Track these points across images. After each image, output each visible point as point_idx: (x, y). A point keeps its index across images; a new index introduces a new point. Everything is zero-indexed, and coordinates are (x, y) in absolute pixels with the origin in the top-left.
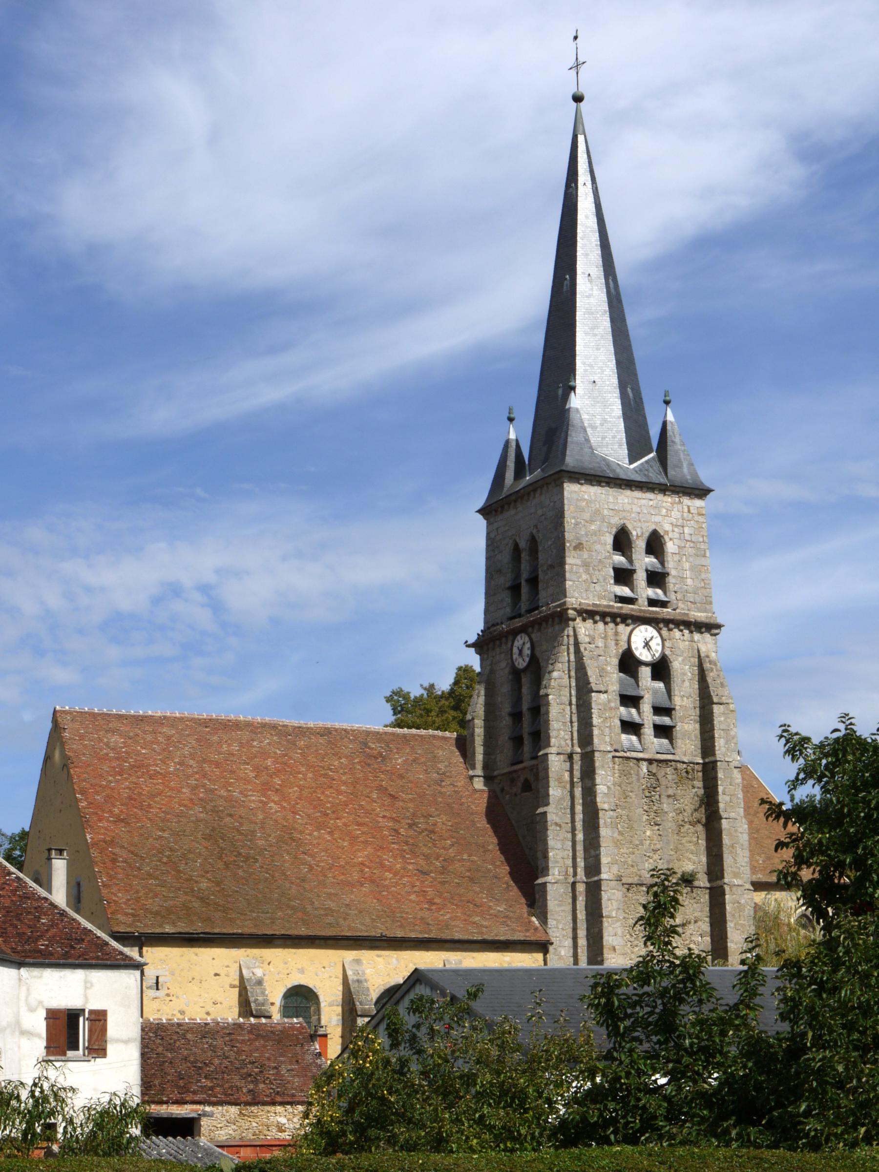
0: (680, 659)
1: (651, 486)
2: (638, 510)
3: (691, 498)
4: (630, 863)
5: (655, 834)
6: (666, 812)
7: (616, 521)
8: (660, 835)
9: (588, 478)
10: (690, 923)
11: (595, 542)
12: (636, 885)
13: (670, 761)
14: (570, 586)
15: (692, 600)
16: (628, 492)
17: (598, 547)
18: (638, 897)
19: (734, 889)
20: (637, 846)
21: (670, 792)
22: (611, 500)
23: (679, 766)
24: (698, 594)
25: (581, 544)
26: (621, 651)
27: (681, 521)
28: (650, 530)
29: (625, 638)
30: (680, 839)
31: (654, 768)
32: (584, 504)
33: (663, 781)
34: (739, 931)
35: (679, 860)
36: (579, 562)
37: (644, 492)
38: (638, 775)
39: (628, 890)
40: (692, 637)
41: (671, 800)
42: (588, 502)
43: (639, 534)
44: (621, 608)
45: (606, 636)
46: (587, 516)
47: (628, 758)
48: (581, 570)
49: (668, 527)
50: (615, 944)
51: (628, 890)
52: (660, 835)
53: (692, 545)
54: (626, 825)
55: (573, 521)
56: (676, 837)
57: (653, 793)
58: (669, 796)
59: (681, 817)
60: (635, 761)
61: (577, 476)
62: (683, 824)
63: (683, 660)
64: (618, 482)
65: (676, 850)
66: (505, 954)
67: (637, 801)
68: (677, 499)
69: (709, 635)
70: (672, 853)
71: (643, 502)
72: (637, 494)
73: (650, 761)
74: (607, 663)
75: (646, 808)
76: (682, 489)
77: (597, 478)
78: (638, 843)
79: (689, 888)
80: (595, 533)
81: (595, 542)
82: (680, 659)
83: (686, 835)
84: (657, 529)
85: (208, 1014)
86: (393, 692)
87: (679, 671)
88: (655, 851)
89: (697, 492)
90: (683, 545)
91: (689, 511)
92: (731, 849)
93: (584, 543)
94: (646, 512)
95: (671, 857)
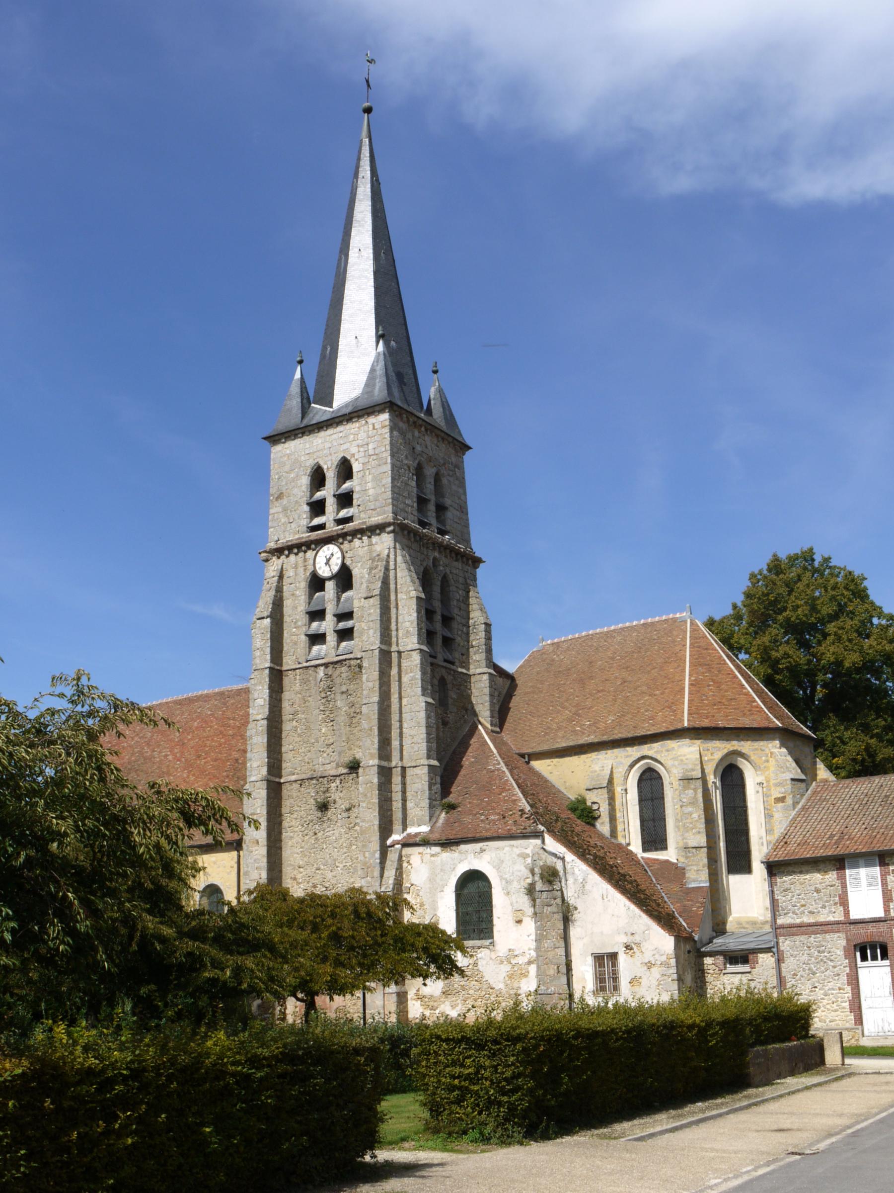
0: (359, 565)
1: (337, 420)
2: (330, 445)
3: (376, 416)
4: (307, 760)
5: (329, 730)
6: (339, 708)
7: (310, 463)
8: (333, 730)
9: (286, 435)
10: (354, 807)
11: (294, 487)
12: (308, 779)
13: (345, 660)
14: (272, 532)
15: (372, 507)
16: (322, 434)
17: (295, 491)
18: (309, 791)
19: (367, 770)
20: (313, 744)
21: (344, 689)
22: (308, 446)
23: (353, 662)
24: (379, 500)
25: (282, 493)
26: (308, 574)
27: (366, 440)
28: (339, 458)
29: (311, 562)
30: (352, 729)
31: (330, 670)
32: (286, 458)
33: (338, 681)
34: (371, 810)
35: (350, 749)
36: (280, 509)
37: (336, 428)
38: (315, 679)
39: (301, 785)
40: (371, 541)
41: (345, 696)
42: (289, 455)
43: (329, 466)
44: (309, 536)
45: (296, 566)
46: (287, 468)
47: (307, 667)
48: (281, 515)
49: (354, 450)
50: (257, 837)
51: (301, 785)
52: (333, 730)
53: (375, 457)
54: (304, 727)
55: (277, 477)
56: (348, 729)
57: (329, 693)
58: (343, 693)
59: (353, 710)
60: (313, 668)
61: (277, 438)
62: (355, 715)
63: (361, 565)
64: (310, 428)
65: (348, 740)
66: (212, 855)
67: (316, 702)
68: (364, 422)
69: (386, 535)
70: (345, 744)
71: (335, 436)
72: (330, 431)
73: (326, 665)
74: (297, 588)
75: (322, 708)
76: (364, 412)
77: (293, 433)
78: (313, 741)
79: (355, 775)
80: (293, 480)
81: (294, 487)
82: (359, 565)
83: (357, 725)
84: (345, 455)
85: (579, 913)
86: (881, 608)
87: (358, 576)
88: (328, 745)
89: (377, 408)
90: (367, 461)
91: (374, 429)
92: (369, 732)
93: (284, 491)
94: (336, 444)
95: (343, 749)
